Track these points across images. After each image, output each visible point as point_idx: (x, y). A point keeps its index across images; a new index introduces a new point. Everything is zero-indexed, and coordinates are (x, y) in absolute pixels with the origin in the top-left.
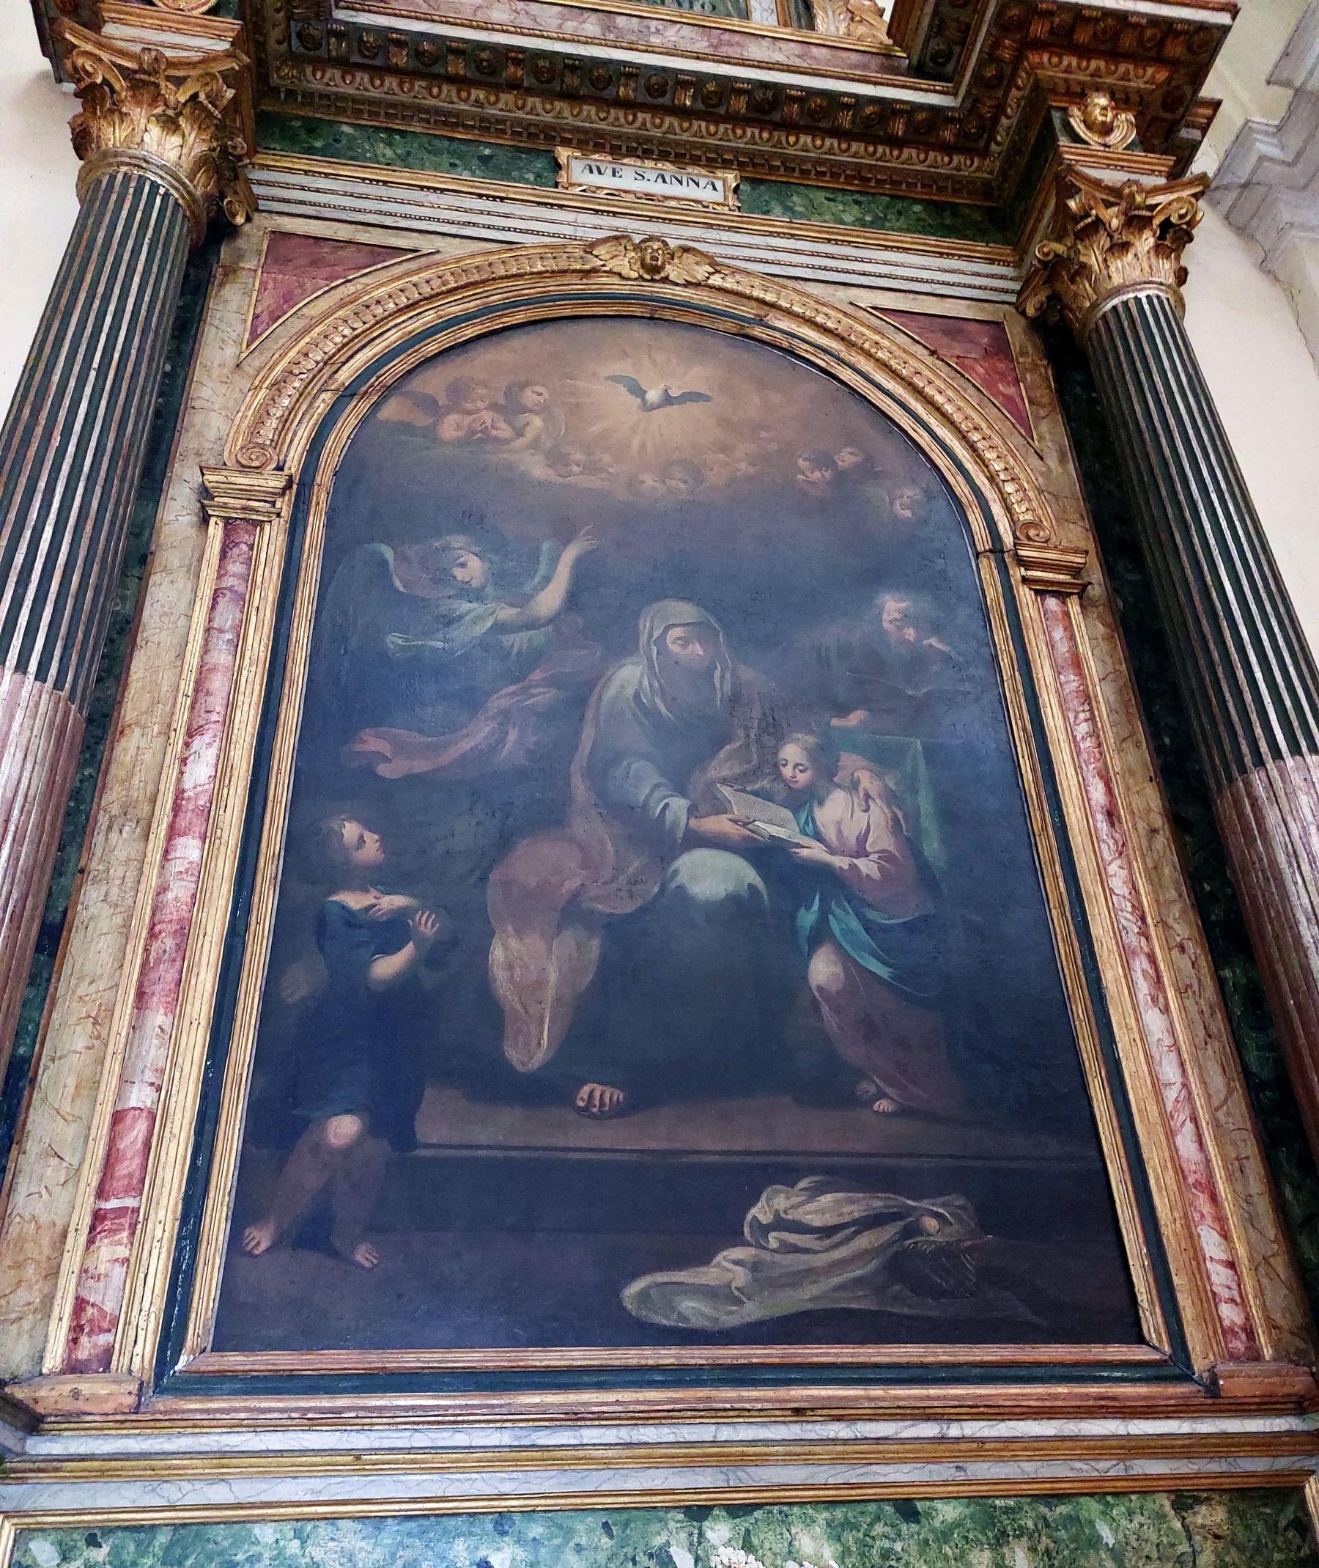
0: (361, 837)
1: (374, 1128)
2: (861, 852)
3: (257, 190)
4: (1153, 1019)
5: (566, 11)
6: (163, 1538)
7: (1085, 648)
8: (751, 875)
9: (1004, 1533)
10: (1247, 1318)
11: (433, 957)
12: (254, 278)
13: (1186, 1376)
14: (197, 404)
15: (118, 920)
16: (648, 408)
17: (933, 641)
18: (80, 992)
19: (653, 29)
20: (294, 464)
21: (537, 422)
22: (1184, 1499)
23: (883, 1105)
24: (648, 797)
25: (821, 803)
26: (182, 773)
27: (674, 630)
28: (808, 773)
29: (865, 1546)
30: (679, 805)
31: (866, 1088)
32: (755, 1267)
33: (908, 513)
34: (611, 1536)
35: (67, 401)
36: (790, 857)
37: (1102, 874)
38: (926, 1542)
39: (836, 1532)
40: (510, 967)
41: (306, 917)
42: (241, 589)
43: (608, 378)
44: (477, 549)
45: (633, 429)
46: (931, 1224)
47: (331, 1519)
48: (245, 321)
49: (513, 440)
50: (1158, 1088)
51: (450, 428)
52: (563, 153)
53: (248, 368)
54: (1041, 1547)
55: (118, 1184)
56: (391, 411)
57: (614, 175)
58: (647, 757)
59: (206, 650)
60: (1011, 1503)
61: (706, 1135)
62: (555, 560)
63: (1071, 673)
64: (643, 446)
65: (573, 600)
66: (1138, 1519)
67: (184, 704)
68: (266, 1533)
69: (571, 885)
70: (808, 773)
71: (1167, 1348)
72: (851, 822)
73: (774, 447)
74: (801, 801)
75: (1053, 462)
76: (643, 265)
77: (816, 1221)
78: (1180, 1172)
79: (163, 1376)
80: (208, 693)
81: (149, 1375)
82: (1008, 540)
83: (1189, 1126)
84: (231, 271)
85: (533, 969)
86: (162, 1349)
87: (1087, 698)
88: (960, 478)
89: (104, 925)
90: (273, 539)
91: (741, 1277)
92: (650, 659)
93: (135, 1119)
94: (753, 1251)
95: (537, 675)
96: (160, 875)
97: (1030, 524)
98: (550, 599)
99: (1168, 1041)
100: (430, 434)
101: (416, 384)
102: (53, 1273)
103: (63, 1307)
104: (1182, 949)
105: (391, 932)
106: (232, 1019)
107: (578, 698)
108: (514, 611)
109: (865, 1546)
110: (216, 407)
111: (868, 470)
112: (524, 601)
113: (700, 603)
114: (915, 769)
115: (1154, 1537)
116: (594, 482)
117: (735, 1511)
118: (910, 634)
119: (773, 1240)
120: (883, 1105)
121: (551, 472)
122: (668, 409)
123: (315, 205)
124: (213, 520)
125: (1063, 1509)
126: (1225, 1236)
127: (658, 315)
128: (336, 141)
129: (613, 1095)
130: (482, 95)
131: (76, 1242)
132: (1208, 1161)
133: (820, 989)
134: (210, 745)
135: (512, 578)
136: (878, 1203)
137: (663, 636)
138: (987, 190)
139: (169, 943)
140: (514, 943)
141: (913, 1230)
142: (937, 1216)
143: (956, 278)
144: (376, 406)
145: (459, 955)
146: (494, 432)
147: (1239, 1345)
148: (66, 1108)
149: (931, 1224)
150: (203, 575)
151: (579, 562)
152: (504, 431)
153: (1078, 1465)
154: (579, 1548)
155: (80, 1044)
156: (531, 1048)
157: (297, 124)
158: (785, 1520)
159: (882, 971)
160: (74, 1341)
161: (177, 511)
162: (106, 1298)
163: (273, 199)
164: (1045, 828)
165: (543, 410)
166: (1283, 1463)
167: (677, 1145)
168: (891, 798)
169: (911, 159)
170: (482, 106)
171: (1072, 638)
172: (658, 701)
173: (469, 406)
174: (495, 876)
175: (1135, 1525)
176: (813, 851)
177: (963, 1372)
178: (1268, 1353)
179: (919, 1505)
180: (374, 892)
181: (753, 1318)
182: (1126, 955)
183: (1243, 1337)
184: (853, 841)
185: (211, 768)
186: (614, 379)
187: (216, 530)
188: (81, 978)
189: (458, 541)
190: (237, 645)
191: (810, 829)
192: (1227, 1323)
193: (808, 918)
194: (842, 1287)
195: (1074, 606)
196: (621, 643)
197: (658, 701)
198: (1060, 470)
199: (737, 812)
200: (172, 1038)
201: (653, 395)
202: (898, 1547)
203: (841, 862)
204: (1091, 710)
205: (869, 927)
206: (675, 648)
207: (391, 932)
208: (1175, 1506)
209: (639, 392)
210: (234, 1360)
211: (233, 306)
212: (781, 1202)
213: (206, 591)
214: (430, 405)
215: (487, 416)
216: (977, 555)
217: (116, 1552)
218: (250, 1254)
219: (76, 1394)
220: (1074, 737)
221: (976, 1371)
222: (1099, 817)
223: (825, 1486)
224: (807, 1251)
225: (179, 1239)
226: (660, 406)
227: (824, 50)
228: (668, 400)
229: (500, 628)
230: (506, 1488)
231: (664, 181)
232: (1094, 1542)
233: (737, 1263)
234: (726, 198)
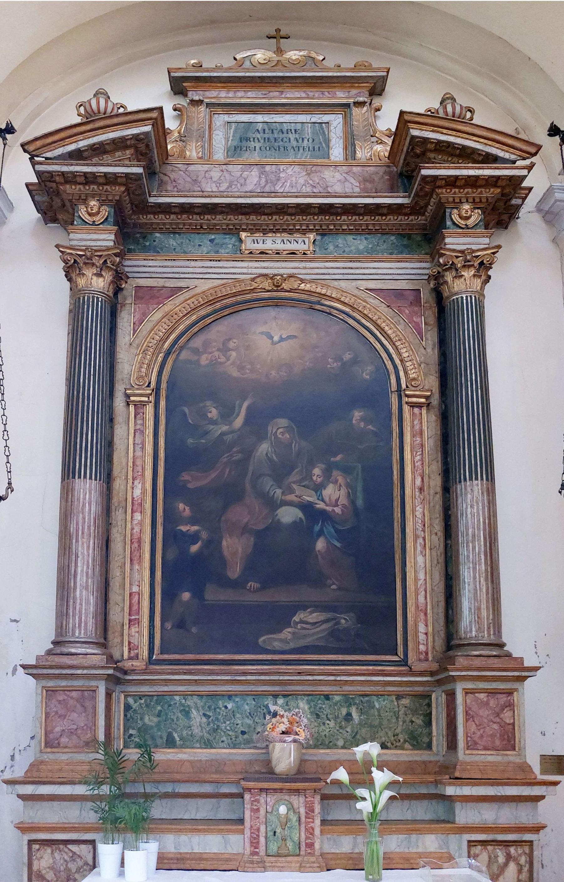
0: (185, 509)
1: (194, 596)
2: (337, 505)
3: (127, 269)
4: (420, 559)
5: (244, 166)
6: (155, 698)
7: (425, 428)
8: (300, 515)
9: (351, 704)
10: (427, 649)
11: (208, 544)
12: (132, 307)
13: (406, 665)
14: (119, 361)
15: (122, 538)
16: (274, 343)
17: (370, 427)
18: (116, 559)
19: (282, 170)
20: (153, 385)
21: (234, 354)
22: (399, 697)
23: (334, 587)
24: (269, 489)
25: (325, 489)
26: (133, 492)
27: (280, 427)
28: (321, 478)
29: (315, 706)
30: (279, 491)
31: (329, 582)
32: (293, 633)
33: (368, 377)
34: (255, 701)
35: (81, 400)
36: (313, 507)
37: (414, 511)
38: (331, 705)
39: (308, 702)
40: (228, 547)
41: (172, 536)
42: (142, 429)
43: (259, 333)
44: (214, 405)
45: (269, 353)
46: (343, 621)
47: (192, 695)
48: (130, 325)
49: (226, 363)
50: (416, 580)
51: (204, 360)
52: (243, 235)
53: (134, 345)
54: (360, 708)
55: (133, 612)
56: (184, 355)
57: (263, 243)
58: (269, 475)
59: (134, 451)
60: (354, 696)
61: (282, 596)
62: (240, 407)
63: (418, 434)
64: (272, 360)
65: (247, 421)
66: (386, 702)
67: (130, 470)
68: (177, 698)
69: (246, 520)
70: (321, 478)
71: (402, 657)
72: (334, 495)
73: (320, 354)
74: (318, 488)
75: (429, 350)
76: (274, 285)
77: (311, 621)
78: (417, 606)
79: (151, 661)
80: (137, 466)
81: (147, 661)
82: (404, 386)
83: (423, 592)
84: (123, 305)
85: (235, 548)
86: (149, 654)
87: (422, 446)
88: (390, 362)
89: (119, 539)
90: (149, 410)
91: (289, 636)
92: (271, 440)
93: (135, 595)
94: (293, 629)
95: (235, 449)
96: (131, 525)
97: (414, 379)
98: (239, 422)
99: (423, 566)
100: (198, 362)
101: (191, 344)
102: (122, 635)
103: (126, 644)
104: (436, 534)
105: (194, 538)
106: (155, 567)
107: (248, 454)
108: (227, 427)
109: (315, 706)
110: (126, 361)
111: (355, 361)
112: (230, 423)
113: (290, 419)
114: (357, 474)
115: (389, 707)
116: (254, 376)
117: (285, 696)
118: (362, 425)
119: (299, 626)
120: (334, 587)
121: (239, 373)
122: (282, 343)
123: (149, 272)
124: (131, 406)
125: (367, 698)
126: (426, 625)
127: (277, 303)
128: (154, 241)
129: (258, 585)
130: (209, 217)
131: (126, 627)
132: (427, 603)
133: (319, 551)
134: (139, 483)
135: (227, 414)
136: (329, 615)
137: (276, 432)
138: (424, 227)
139: (136, 545)
140: (229, 540)
141: (338, 623)
142: (345, 619)
143: (403, 271)
144: (178, 355)
145: (213, 544)
146: (219, 360)
147: (422, 657)
148: (118, 592)
149: (343, 621)
150: (130, 425)
151: (249, 408)
152: (223, 359)
153: (371, 687)
154: (247, 704)
155: (118, 574)
156: (235, 572)
157: (138, 235)
158: (297, 699)
159: (338, 544)
160: (129, 652)
161: (119, 402)
162: (135, 641)
163: (134, 272)
164: (397, 495)
165: (236, 349)
166: (427, 689)
167: (274, 600)
168: (348, 486)
169: (391, 219)
170: (210, 220)
171: (421, 423)
172: (273, 455)
173: (210, 350)
174: (223, 518)
175: (385, 703)
176: (321, 505)
177: (346, 662)
178: (430, 659)
179: (330, 696)
180: (189, 526)
181: (293, 647)
182: (416, 537)
183: (424, 654)
184: (334, 501)
185: (140, 490)
186: (262, 333)
187: (132, 408)
188: (115, 555)
189: (208, 403)
190: (143, 448)
191: (320, 498)
192: (420, 650)
193: (317, 528)
194: (317, 639)
195: (424, 411)
196: (261, 437)
197: (273, 455)
198: (431, 353)
199: (297, 493)
200: (140, 572)
201: (276, 338)
202: (324, 706)
203: (329, 509)
204: (422, 451)
205: (337, 531)
206: (280, 436)
207: (194, 538)
208: (396, 698)
209: (271, 338)
210: (166, 657)
211: (125, 320)
212: (302, 616)
213: (132, 431)
214: (196, 351)
215: (216, 354)
216: (392, 392)
217: (146, 701)
218: (167, 630)
219: (132, 665)
220: (414, 461)
221: (349, 662)
222: (417, 490)
223: (307, 691)
224: (308, 629)
225: (150, 626)
226: (279, 342)
227: (359, 168)
228: (282, 340)
229: (223, 434)
230: (230, 689)
231: (284, 243)
232: (373, 707)
233: (289, 632)
234: (309, 247)
